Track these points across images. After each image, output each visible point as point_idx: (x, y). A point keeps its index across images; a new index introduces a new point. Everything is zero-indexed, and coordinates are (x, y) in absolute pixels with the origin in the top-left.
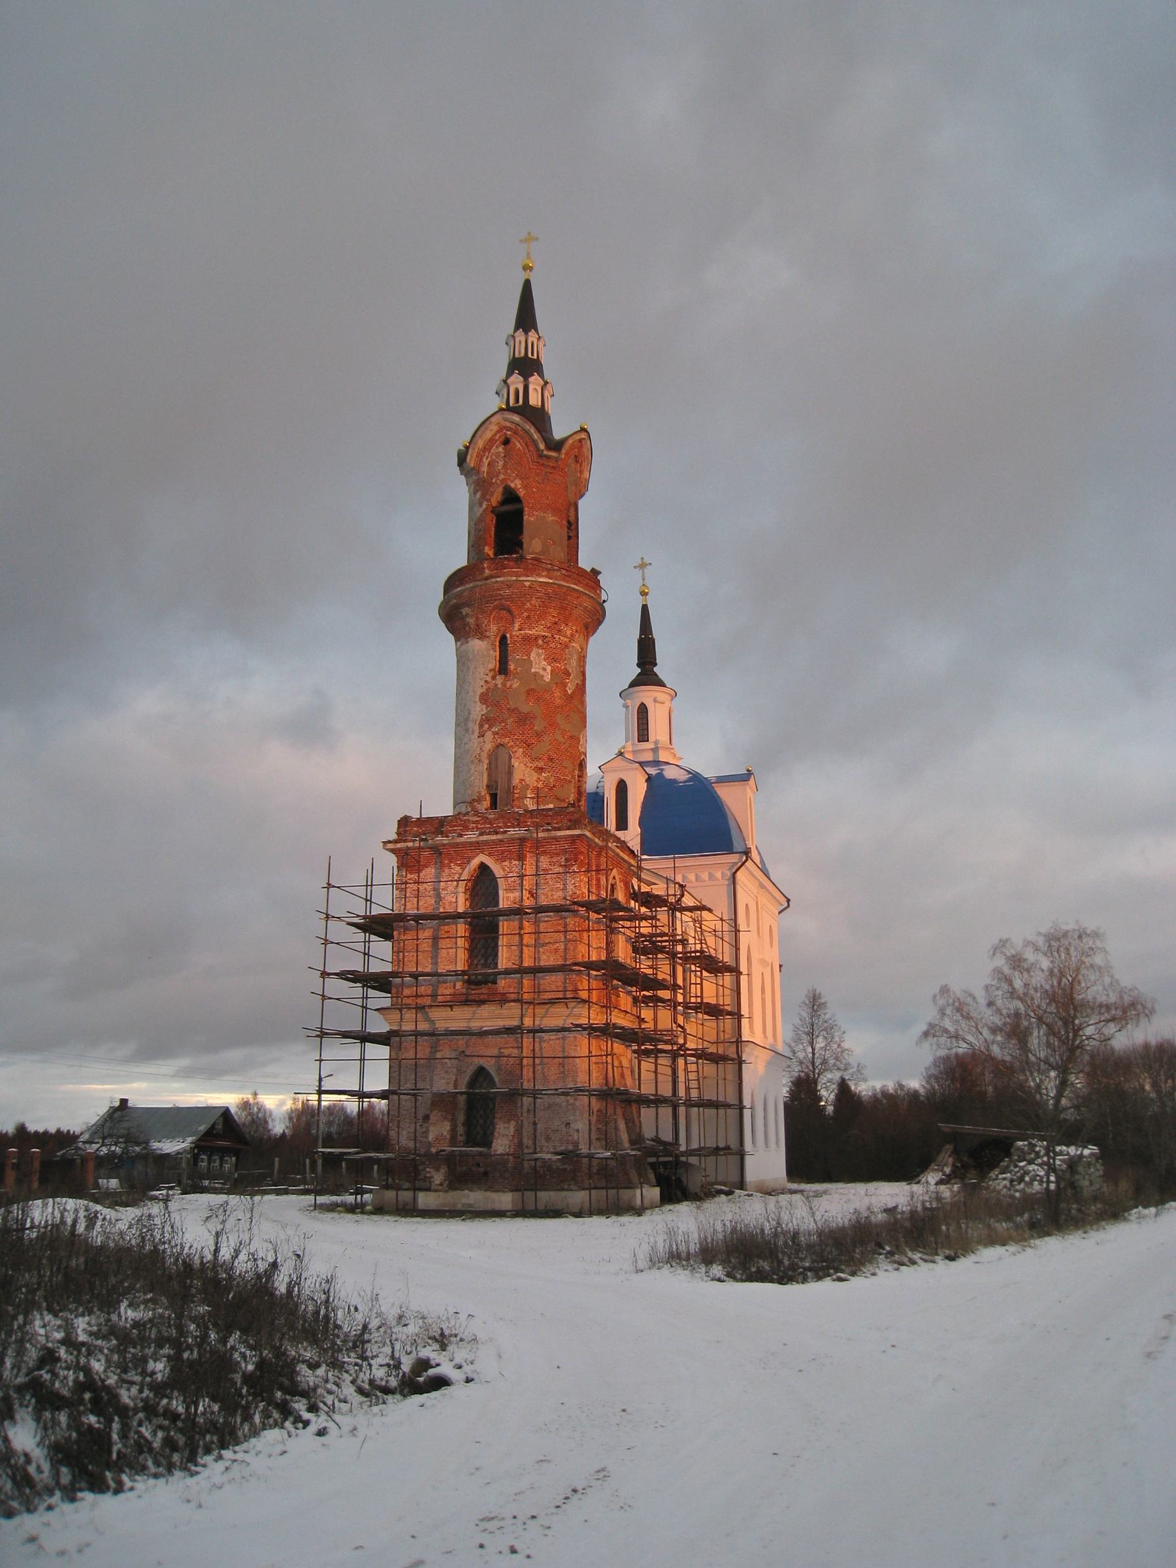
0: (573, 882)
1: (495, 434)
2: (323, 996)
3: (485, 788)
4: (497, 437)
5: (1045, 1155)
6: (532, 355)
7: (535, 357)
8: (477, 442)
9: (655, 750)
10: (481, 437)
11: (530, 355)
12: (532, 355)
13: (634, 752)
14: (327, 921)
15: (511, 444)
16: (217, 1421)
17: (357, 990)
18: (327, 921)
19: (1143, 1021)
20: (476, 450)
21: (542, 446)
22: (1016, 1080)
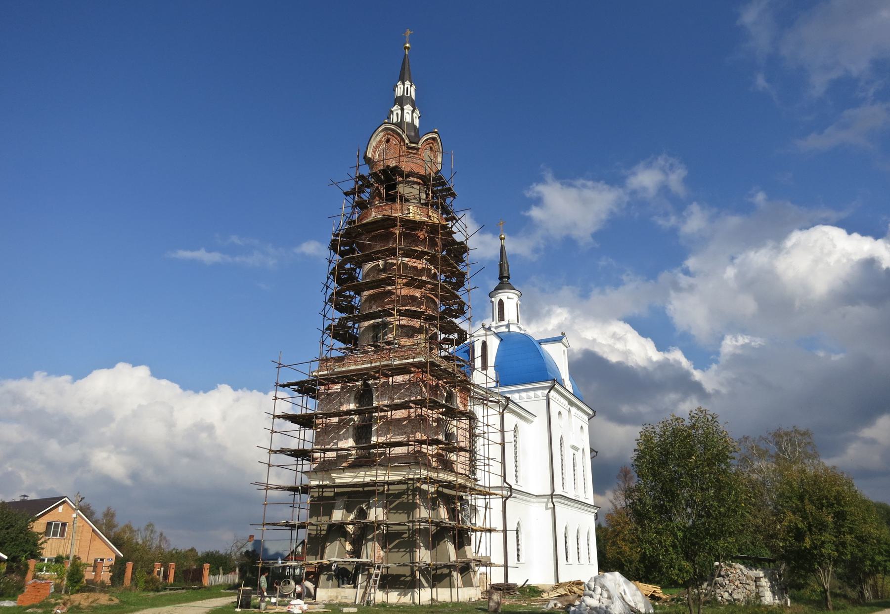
0: (416, 390)
1: (382, 138)
2: (269, 465)
3: (371, 338)
4: (383, 139)
5: (701, 593)
6: (407, 94)
7: (409, 95)
8: (372, 144)
9: (508, 326)
10: (374, 140)
11: (405, 94)
12: (407, 94)
13: (496, 328)
14: (273, 419)
15: (390, 142)
16: (843, 528)
17: (293, 460)
18: (273, 419)
19: (666, 353)
20: (372, 148)
21: (407, 141)
22: (107, 531)
